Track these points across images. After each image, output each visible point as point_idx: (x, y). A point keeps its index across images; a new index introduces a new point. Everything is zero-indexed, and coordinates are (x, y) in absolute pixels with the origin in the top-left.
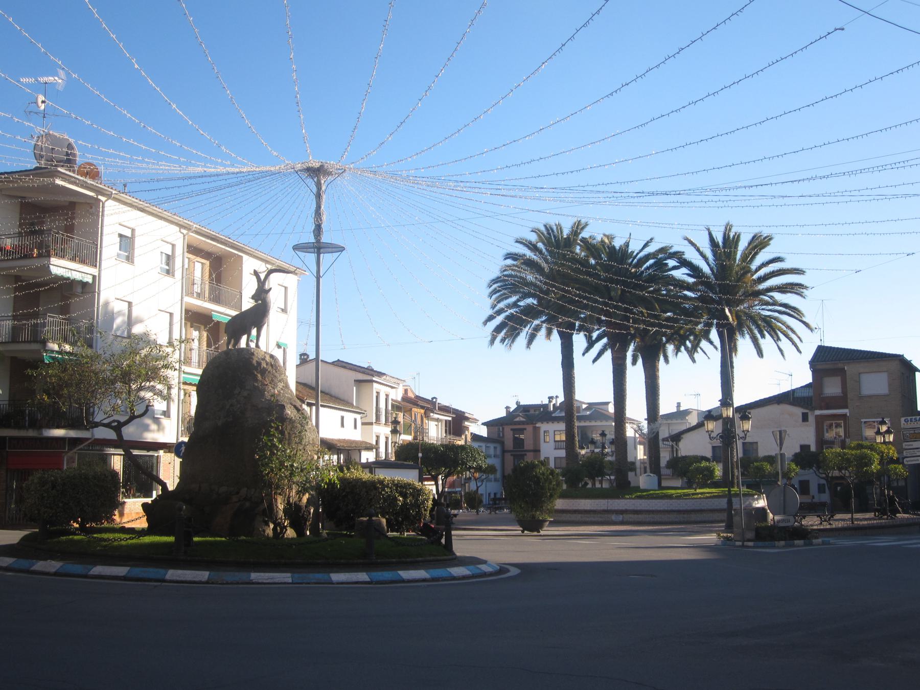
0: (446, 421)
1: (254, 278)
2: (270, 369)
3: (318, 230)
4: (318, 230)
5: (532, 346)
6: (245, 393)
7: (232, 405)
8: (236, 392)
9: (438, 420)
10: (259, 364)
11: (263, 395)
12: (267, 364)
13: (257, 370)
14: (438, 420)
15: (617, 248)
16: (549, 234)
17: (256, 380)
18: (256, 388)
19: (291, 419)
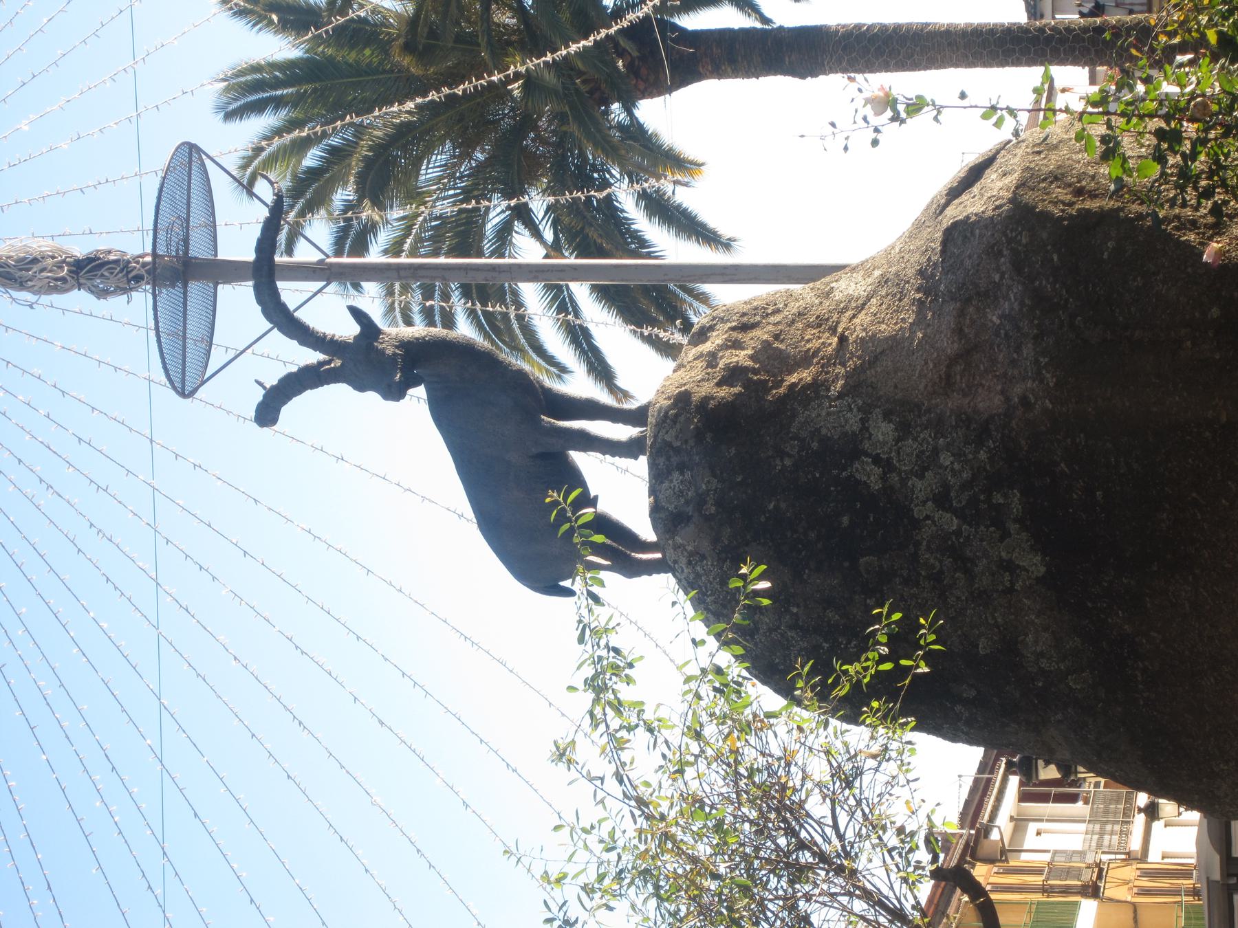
0: (1024, 797)
1: (292, 411)
2: (762, 334)
3: (95, 272)
4: (95, 272)
5: (725, 231)
6: (883, 431)
7: (942, 500)
8: (871, 475)
9: (1019, 823)
10: (733, 374)
11: (894, 344)
12: (737, 345)
13: (763, 387)
14: (1019, 823)
15: (419, 393)
16: (278, 103)
17: (816, 388)
18: (855, 386)
19: (1021, 185)
